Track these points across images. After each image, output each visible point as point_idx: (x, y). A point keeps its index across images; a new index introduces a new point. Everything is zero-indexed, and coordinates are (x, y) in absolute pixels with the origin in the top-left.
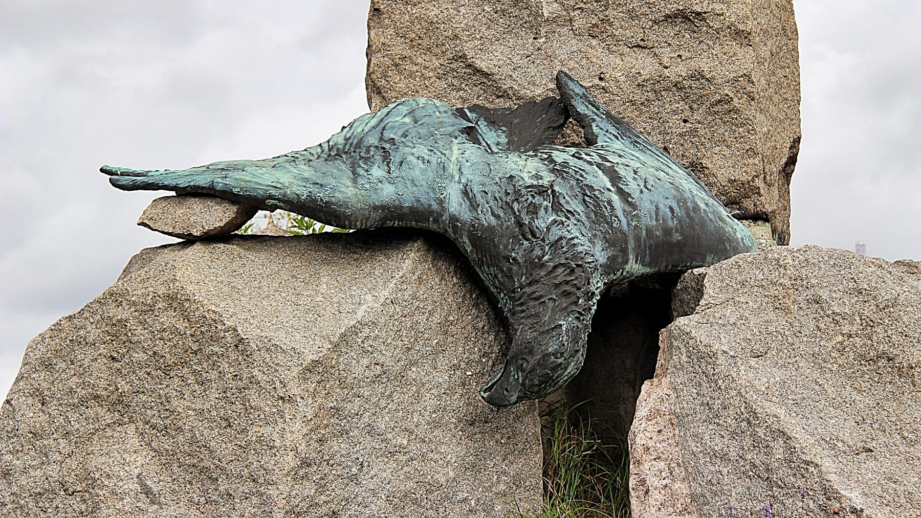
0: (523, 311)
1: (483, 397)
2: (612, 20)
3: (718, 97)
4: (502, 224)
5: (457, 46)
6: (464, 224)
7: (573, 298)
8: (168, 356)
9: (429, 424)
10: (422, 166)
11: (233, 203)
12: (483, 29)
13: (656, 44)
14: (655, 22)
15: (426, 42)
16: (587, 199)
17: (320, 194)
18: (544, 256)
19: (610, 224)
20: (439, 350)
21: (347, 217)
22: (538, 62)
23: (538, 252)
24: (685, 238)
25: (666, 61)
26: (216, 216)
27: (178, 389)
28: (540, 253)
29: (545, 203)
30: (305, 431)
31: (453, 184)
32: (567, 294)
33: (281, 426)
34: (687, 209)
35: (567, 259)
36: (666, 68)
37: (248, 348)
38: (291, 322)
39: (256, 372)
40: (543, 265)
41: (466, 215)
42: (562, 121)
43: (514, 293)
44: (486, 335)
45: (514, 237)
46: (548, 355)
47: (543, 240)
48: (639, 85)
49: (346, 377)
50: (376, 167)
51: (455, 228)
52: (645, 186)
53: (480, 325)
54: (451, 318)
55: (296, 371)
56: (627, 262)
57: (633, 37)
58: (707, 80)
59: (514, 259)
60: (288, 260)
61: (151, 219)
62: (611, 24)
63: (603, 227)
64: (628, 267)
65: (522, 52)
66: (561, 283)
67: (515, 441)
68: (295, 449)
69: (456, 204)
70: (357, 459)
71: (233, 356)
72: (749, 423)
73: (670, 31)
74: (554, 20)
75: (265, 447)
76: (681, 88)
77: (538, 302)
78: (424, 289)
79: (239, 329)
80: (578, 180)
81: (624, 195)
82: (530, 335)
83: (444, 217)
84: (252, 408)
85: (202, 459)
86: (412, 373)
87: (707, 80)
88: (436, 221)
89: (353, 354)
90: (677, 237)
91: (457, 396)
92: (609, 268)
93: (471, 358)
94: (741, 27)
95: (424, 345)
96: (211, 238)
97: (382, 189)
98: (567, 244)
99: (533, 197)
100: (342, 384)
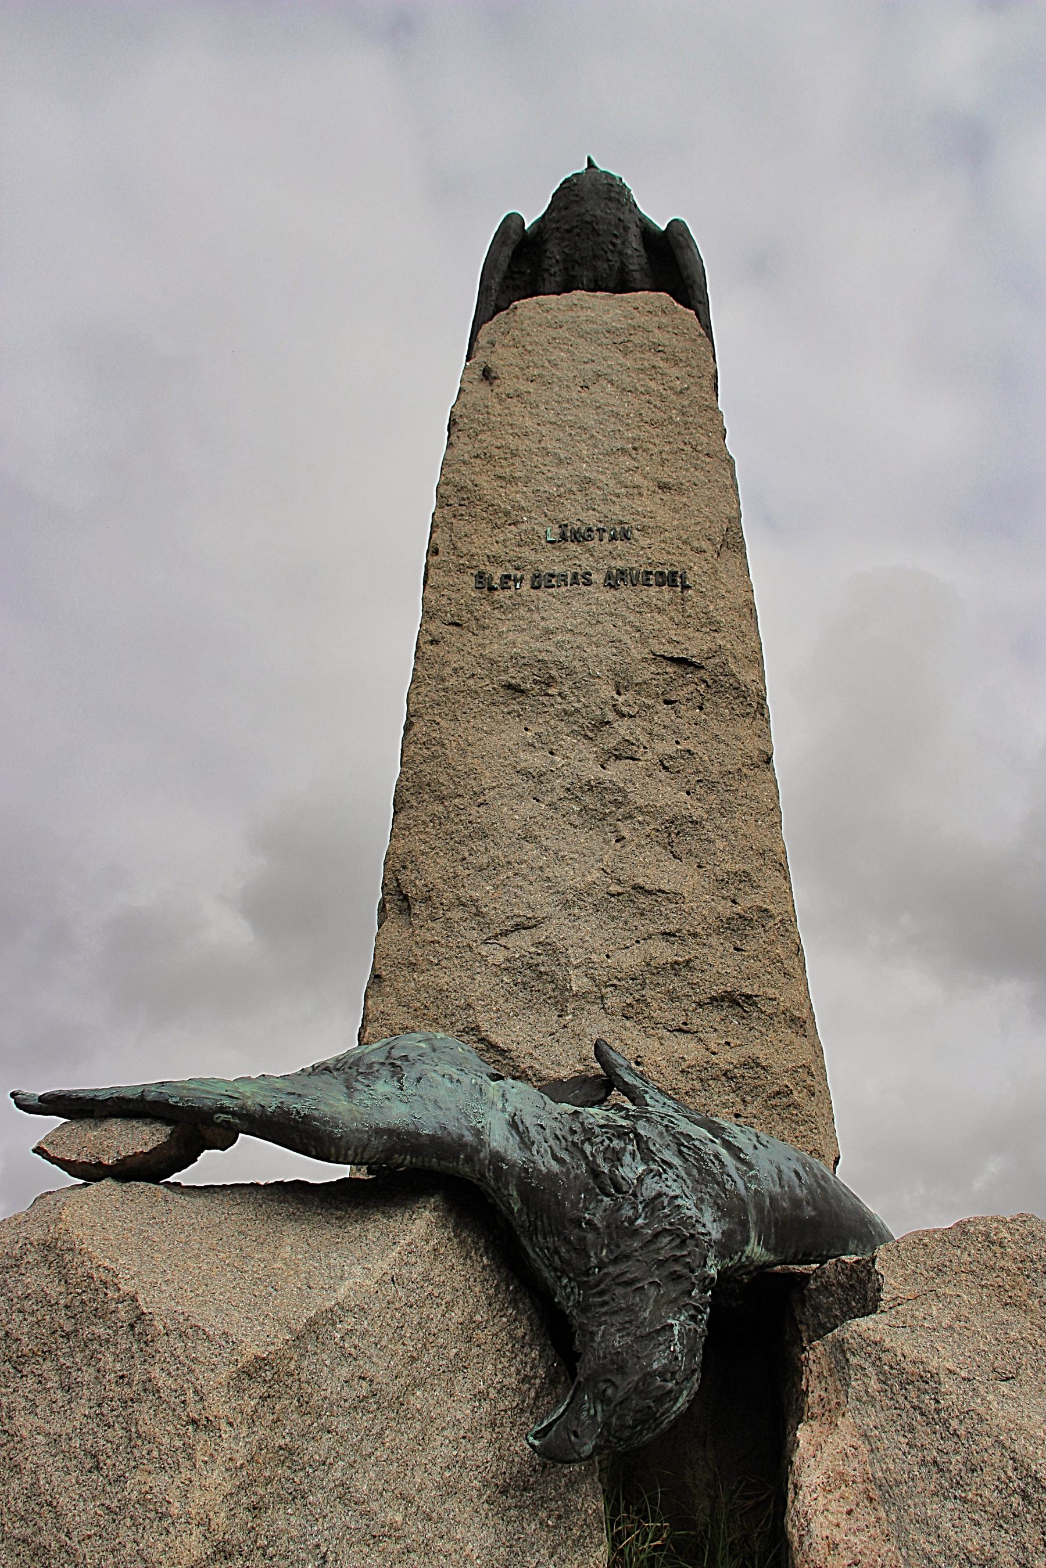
0: (604, 1303)
1: (532, 1445)
2: (649, 1000)
3: (776, 1088)
4: (568, 1172)
5: (469, 1016)
6: (512, 1166)
7: (686, 1285)
8: (25, 1339)
9: (438, 1488)
10: (449, 1085)
11: (168, 1123)
12: (501, 1001)
13: (701, 1029)
14: (700, 1005)
15: (432, 1012)
16: (685, 1150)
17: (295, 1105)
18: (637, 1219)
19: (722, 1185)
20: (459, 1366)
21: (335, 1141)
22: (563, 1040)
23: (627, 1212)
24: (820, 1214)
25: (713, 1047)
26: (142, 1138)
27: (31, 1396)
28: (631, 1213)
29: (630, 1147)
30: (228, 1487)
31: (494, 1112)
32: (676, 1278)
33: (186, 1473)
34: (815, 1176)
35: (671, 1224)
36: (714, 1053)
37: (150, 1330)
38: (228, 1294)
39: (156, 1372)
40: (635, 1233)
41: (515, 1155)
42: (602, 1095)
43: (588, 1275)
44: (527, 1350)
45: (587, 1191)
46: (652, 1374)
47: (634, 1195)
48: (683, 1071)
49: (311, 1395)
50: (382, 1082)
51: (498, 1170)
52: (758, 1141)
53: (520, 1332)
54: (478, 1318)
55: (224, 1373)
56: (747, 1243)
57: (673, 1020)
58: (763, 1068)
59: (589, 1222)
60: (236, 1210)
61: (52, 1143)
62: (648, 1005)
63: (713, 1189)
64: (748, 1250)
65: (545, 1030)
66: (667, 1260)
67: (568, 1522)
68: (205, 1523)
69: (499, 1138)
70: (318, 1546)
71: (124, 1344)
72: (1025, 1496)
73: (716, 1016)
74: (584, 996)
75: (152, 1515)
76: (732, 1078)
77: (629, 1289)
78: (441, 1267)
79: (140, 1298)
80: (667, 1126)
81: (735, 1151)
82: (618, 1341)
83: (482, 1155)
84: (139, 1436)
85: (40, 1529)
86: (417, 1400)
87: (763, 1068)
88: (469, 1159)
89: (324, 1356)
90: (809, 1212)
91: (483, 1443)
92: (727, 1247)
93: (506, 1382)
94: (797, 1014)
95: (437, 1355)
96: (127, 1171)
97: (390, 1108)
98: (669, 1204)
99: (611, 1140)
100: (303, 1404)
